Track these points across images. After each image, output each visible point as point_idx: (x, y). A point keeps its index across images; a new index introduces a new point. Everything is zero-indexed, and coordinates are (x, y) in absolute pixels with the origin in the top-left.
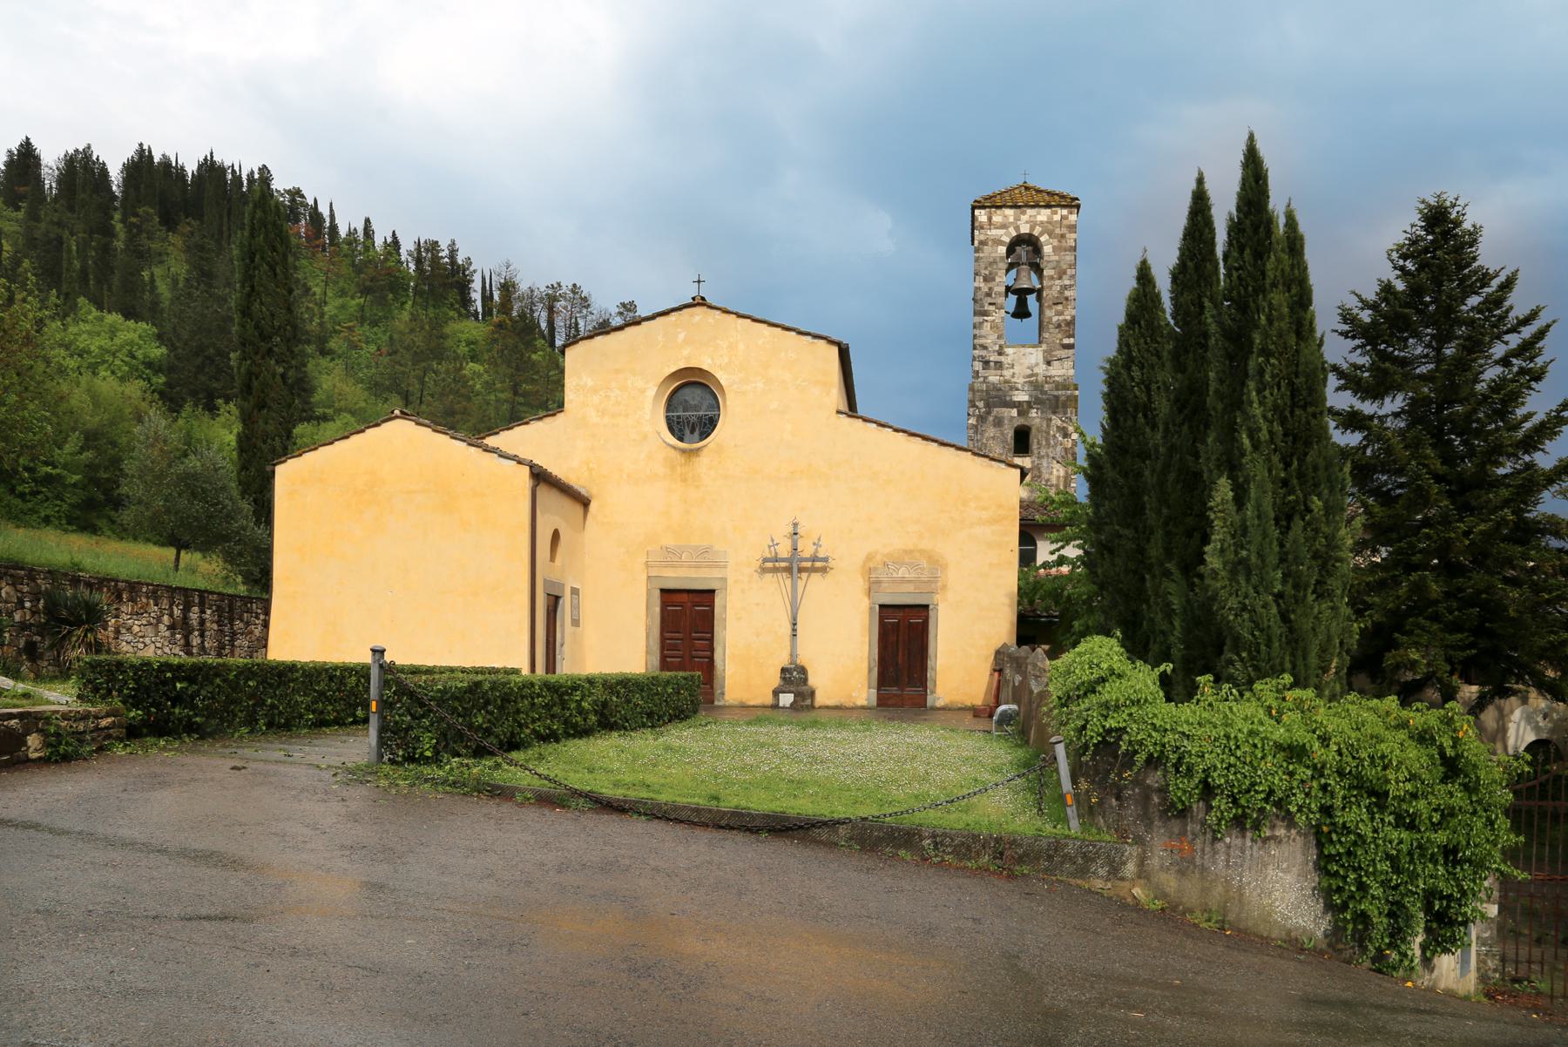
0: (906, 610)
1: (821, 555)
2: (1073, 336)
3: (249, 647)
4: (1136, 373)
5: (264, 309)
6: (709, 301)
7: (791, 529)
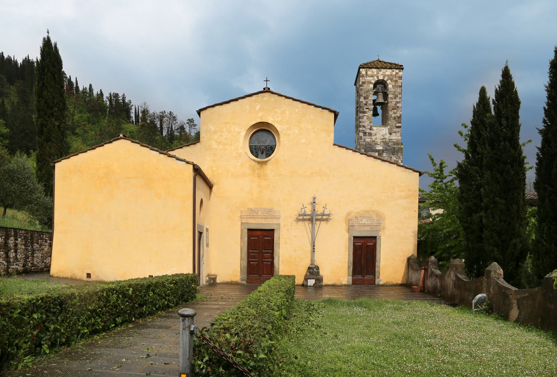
0: (366, 239)
1: (326, 213)
2: (400, 123)
3: (41, 257)
4: (504, 122)
5: (49, 94)
6: (271, 90)
7: (311, 200)
